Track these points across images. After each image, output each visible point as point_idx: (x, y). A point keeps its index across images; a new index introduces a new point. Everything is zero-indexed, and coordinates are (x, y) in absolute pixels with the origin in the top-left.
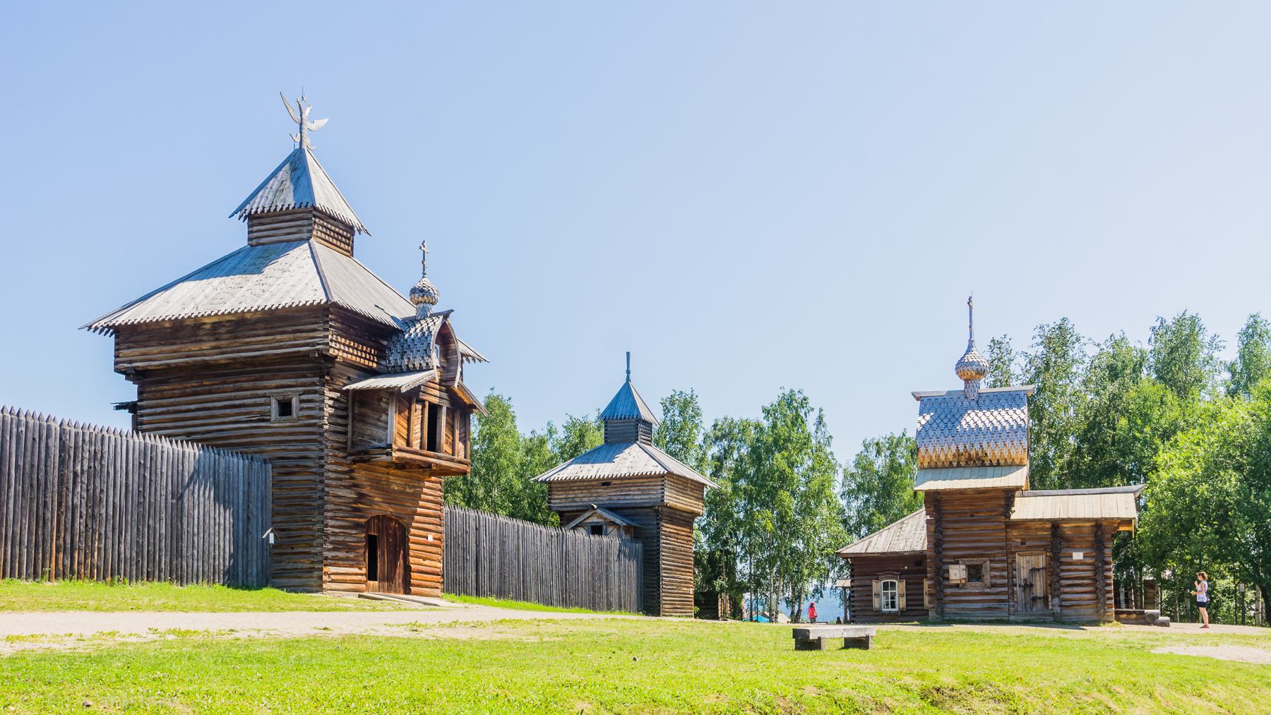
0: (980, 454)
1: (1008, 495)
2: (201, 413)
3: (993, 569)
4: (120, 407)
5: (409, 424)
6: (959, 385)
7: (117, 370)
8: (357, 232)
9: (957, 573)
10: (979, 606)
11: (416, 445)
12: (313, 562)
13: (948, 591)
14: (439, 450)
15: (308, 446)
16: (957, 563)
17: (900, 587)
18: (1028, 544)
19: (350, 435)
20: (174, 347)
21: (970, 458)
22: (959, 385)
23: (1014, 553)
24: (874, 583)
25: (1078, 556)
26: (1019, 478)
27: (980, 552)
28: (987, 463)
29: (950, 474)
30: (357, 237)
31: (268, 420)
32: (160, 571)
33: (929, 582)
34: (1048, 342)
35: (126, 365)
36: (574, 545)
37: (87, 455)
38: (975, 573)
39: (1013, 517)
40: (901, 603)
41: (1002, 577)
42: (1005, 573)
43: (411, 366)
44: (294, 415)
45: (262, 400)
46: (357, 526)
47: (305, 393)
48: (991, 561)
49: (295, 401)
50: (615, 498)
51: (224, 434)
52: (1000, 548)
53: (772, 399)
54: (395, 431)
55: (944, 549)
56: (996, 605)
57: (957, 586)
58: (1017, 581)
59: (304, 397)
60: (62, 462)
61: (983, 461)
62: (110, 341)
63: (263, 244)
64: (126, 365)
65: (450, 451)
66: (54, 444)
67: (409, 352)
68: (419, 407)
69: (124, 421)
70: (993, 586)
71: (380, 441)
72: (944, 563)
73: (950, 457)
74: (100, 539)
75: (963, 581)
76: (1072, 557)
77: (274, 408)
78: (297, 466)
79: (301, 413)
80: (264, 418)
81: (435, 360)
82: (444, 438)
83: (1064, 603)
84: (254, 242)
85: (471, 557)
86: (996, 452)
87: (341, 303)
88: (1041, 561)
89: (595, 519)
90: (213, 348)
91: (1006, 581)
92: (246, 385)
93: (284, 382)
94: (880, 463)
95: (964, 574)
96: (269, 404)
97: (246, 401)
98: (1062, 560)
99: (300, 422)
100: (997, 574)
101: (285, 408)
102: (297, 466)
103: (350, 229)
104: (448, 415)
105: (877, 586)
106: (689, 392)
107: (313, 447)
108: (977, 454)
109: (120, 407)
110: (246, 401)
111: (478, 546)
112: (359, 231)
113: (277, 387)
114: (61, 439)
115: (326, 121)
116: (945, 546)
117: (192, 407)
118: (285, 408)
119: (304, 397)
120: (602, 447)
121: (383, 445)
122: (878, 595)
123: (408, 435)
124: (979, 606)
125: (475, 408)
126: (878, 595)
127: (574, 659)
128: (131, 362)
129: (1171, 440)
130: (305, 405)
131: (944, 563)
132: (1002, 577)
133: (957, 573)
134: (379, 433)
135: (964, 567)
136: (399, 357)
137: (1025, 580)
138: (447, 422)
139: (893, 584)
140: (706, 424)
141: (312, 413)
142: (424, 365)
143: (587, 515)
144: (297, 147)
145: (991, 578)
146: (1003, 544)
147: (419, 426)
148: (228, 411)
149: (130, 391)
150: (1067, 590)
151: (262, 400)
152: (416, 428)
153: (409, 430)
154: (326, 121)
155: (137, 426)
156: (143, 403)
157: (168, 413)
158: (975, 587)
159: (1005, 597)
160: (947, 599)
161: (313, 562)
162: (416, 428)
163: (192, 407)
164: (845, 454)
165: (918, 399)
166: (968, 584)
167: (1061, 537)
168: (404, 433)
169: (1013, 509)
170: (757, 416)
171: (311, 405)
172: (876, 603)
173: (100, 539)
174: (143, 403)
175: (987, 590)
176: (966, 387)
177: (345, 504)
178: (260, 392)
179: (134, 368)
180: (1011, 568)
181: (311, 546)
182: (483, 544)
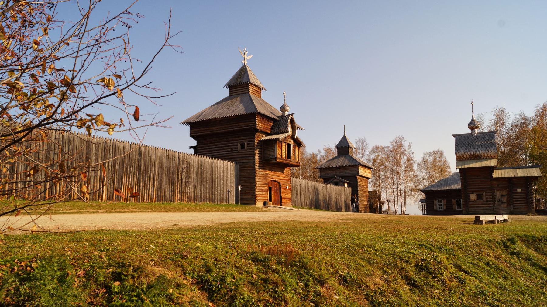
0: (479, 155)
1: (491, 169)
2: (216, 149)
3: (486, 195)
4: (191, 148)
5: (282, 151)
6: (469, 131)
7: (191, 136)
8: (262, 90)
9: (473, 197)
10: (482, 208)
11: (284, 156)
12: (252, 196)
13: (470, 203)
14: (291, 159)
15: (250, 158)
16: (473, 193)
17: (444, 202)
18: (500, 186)
19: (263, 155)
20: (207, 129)
21: (475, 157)
22: (469, 131)
23: (494, 189)
24: (434, 201)
25: (519, 190)
26: (493, 163)
27: (482, 189)
28: (482, 158)
29: (468, 162)
30: (263, 92)
31: (237, 150)
32: (207, 199)
33: (463, 200)
34: (497, 115)
35: (193, 134)
36: (330, 189)
37: (185, 163)
38: (479, 197)
39: (494, 176)
40: (444, 207)
41: (491, 198)
42: (491, 197)
43: (281, 131)
44: (246, 148)
45: (236, 144)
46: (265, 184)
47: (249, 141)
48: (486, 193)
49: (246, 144)
50: (342, 173)
51: (224, 155)
52: (489, 188)
53: (393, 139)
54: (278, 153)
55: (468, 189)
56: (488, 208)
57: (473, 201)
58: (496, 199)
59: (249, 143)
60: (179, 165)
61: (480, 158)
62: (188, 128)
63: (234, 95)
64: (193, 134)
65: (294, 159)
66: (176, 159)
67: (281, 127)
68: (284, 144)
69: (192, 151)
70: (487, 201)
71: (273, 156)
72: (468, 194)
73: (468, 156)
74: (189, 189)
75: (476, 200)
76: (517, 190)
77: (239, 146)
78: (247, 165)
79: (248, 148)
80: (236, 149)
81: (290, 129)
82: (292, 155)
83: (515, 207)
84: (231, 94)
85: (299, 193)
86: (485, 154)
87: (260, 112)
88: (505, 192)
89: (335, 180)
90: (220, 128)
91: (492, 200)
92: (230, 139)
93: (242, 138)
94: (430, 159)
95: (476, 197)
96: (238, 145)
97: (230, 145)
98: (513, 192)
99: (248, 151)
100: (488, 197)
101: (243, 146)
102: (247, 165)
103: (260, 88)
104: (293, 147)
105: (436, 202)
106: (494, 116)
107: (252, 159)
108: (478, 155)
109: (191, 148)
110: (230, 145)
111: (301, 190)
112: (263, 89)
113: (240, 140)
114: (178, 158)
115: (252, 56)
116: (468, 187)
117: (214, 147)
118: (243, 146)
119: (249, 143)
120: (337, 156)
121: (274, 157)
122: (436, 205)
123: (282, 154)
124: (482, 208)
125: (302, 145)
126: (436, 205)
127: (325, 228)
128: (195, 134)
129: (500, 154)
130: (249, 145)
131: (468, 194)
132: (491, 198)
133: (473, 197)
134: (272, 153)
135: (476, 195)
136: (277, 129)
137: (499, 199)
138: (293, 149)
139: (441, 201)
140: (370, 148)
141: (251, 147)
142: (286, 131)
143: (333, 179)
144: (243, 64)
145: (486, 198)
146: (490, 186)
147: (285, 151)
148: (225, 148)
149: (194, 143)
150: (515, 202)
151: (236, 144)
152: (284, 151)
153: (282, 152)
154: (252, 56)
155: (196, 153)
156: (198, 146)
157: (206, 149)
158: (480, 202)
159: (492, 205)
160: (470, 206)
161: (252, 196)
162: (284, 151)
163: (214, 147)
164: (418, 157)
165: (454, 137)
166: (478, 201)
167: (41, 215)
168: (280, 153)
169: (493, 174)
170: (388, 145)
171: (251, 145)
172: (435, 208)
173: (189, 189)
174: (198, 146)
175: (485, 203)
176: (472, 132)
177: (263, 177)
178: (235, 141)
179: (196, 135)
180: (494, 195)
181: (251, 190)
182: (302, 189)
